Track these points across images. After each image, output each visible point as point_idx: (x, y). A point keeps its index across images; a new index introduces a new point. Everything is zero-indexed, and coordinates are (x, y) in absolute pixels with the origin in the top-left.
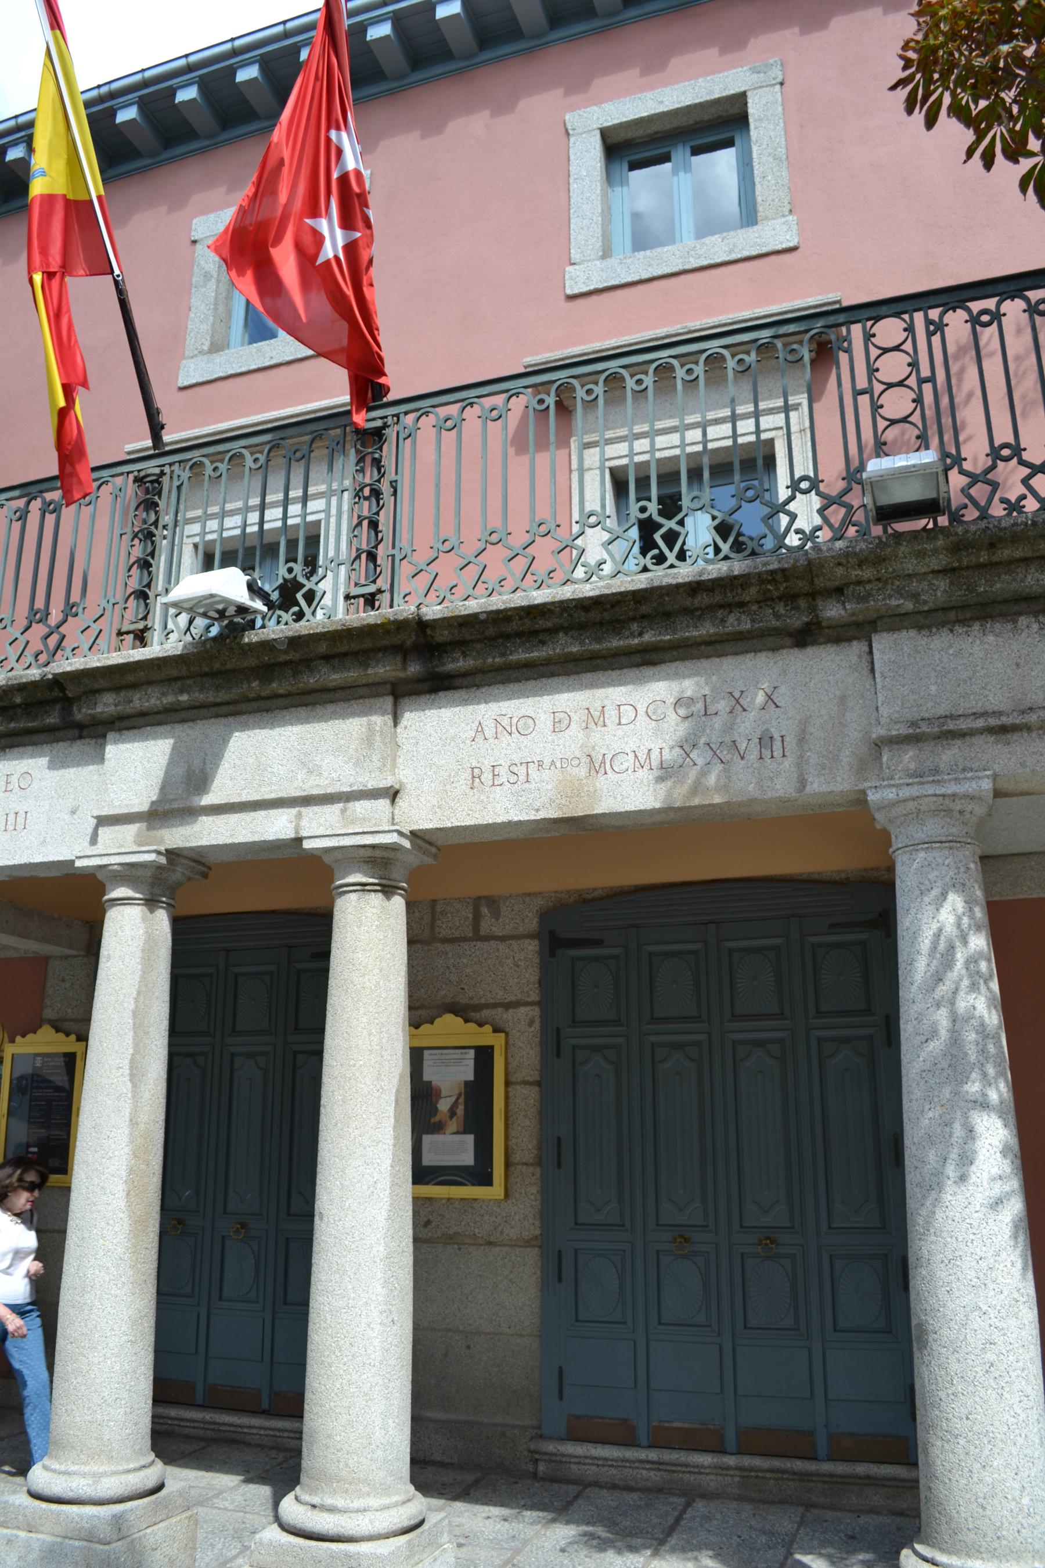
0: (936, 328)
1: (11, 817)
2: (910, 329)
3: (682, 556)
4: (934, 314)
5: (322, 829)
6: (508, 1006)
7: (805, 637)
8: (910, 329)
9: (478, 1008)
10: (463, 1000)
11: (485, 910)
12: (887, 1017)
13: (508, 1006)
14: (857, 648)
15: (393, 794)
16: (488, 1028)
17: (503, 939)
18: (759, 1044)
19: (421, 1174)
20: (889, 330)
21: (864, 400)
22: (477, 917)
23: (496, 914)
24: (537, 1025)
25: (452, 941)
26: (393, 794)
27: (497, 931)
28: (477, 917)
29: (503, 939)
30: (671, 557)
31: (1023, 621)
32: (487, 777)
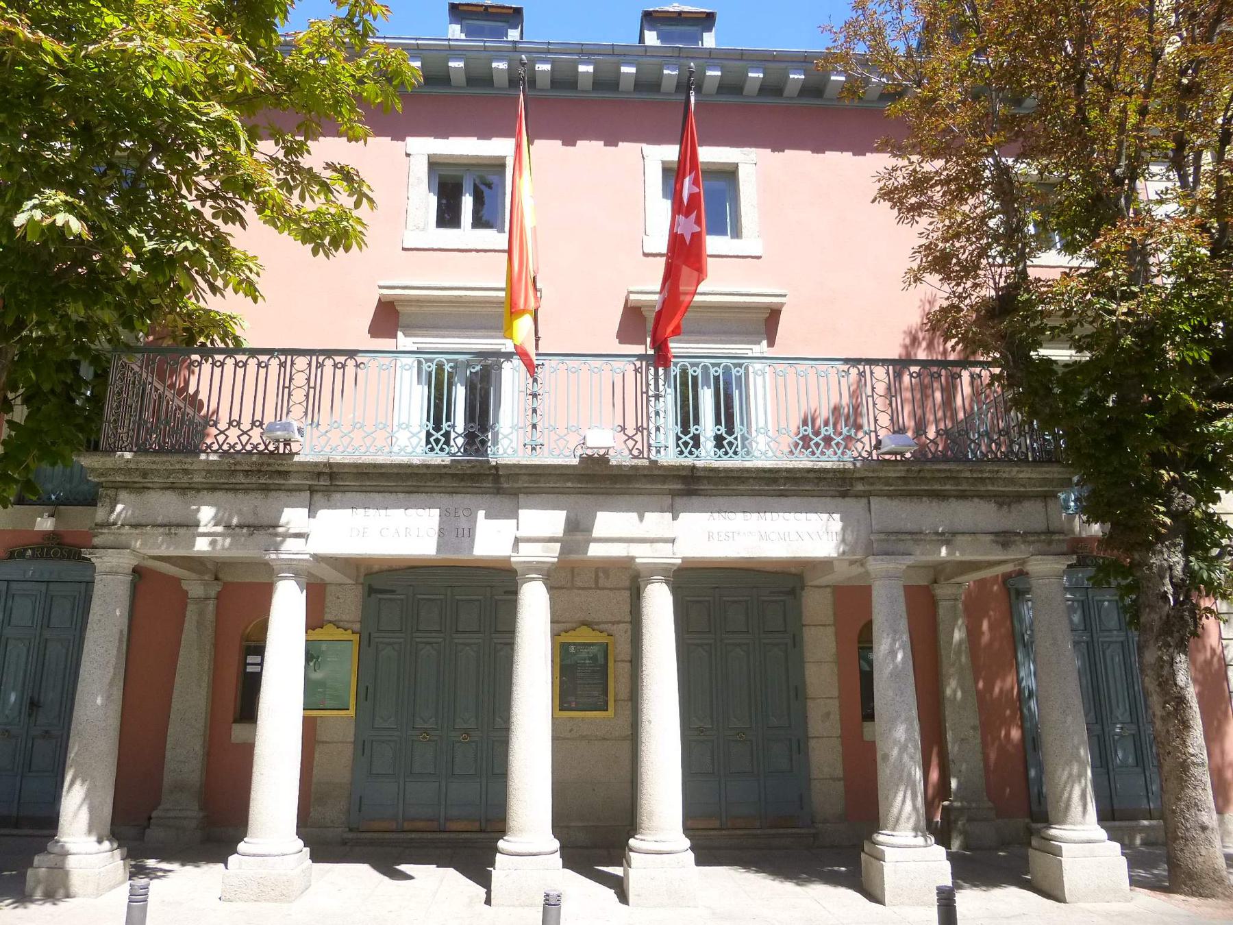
0: (320, 366)
1: (460, 531)
2: (310, 364)
3: (748, 453)
4: (321, 359)
5: (644, 554)
6: (613, 623)
7: (844, 495)
8: (310, 364)
9: (598, 623)
10: (589, 619)
11: (601, 574)
12: (794, 636)
13: (613, 623)
14: (864, 501)
15: (673, 541)
16: (605, 634)
17: (610, 589)
18: (739, 645)
19: (42, 557)
20: (301, 362)
21: (312, 385)
22: (597, 577)
23: (607, 577)
24: (629, 633)
25: (583, 589)
26: (673, 541)
27: (608, 585)
28: (597, 577)
29: (610, 589)
30: (731, 452)
31: (924, 499)
32: (715, 536)
